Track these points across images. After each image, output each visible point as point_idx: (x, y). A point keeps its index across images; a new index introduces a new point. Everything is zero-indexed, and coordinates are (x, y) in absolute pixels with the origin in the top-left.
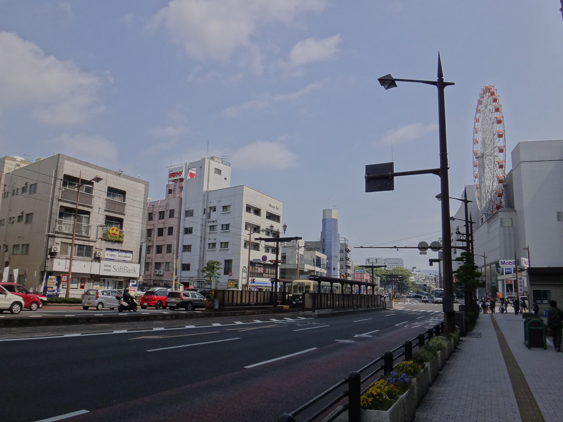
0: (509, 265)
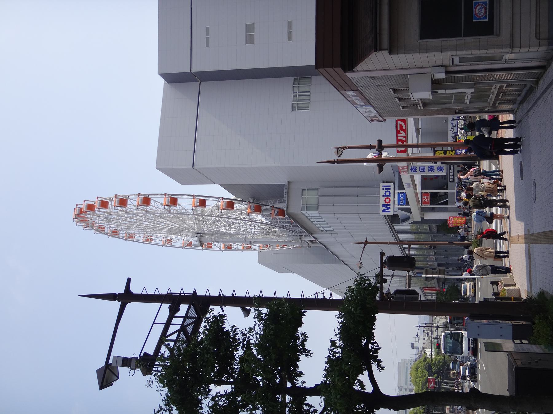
0: (391, 198)
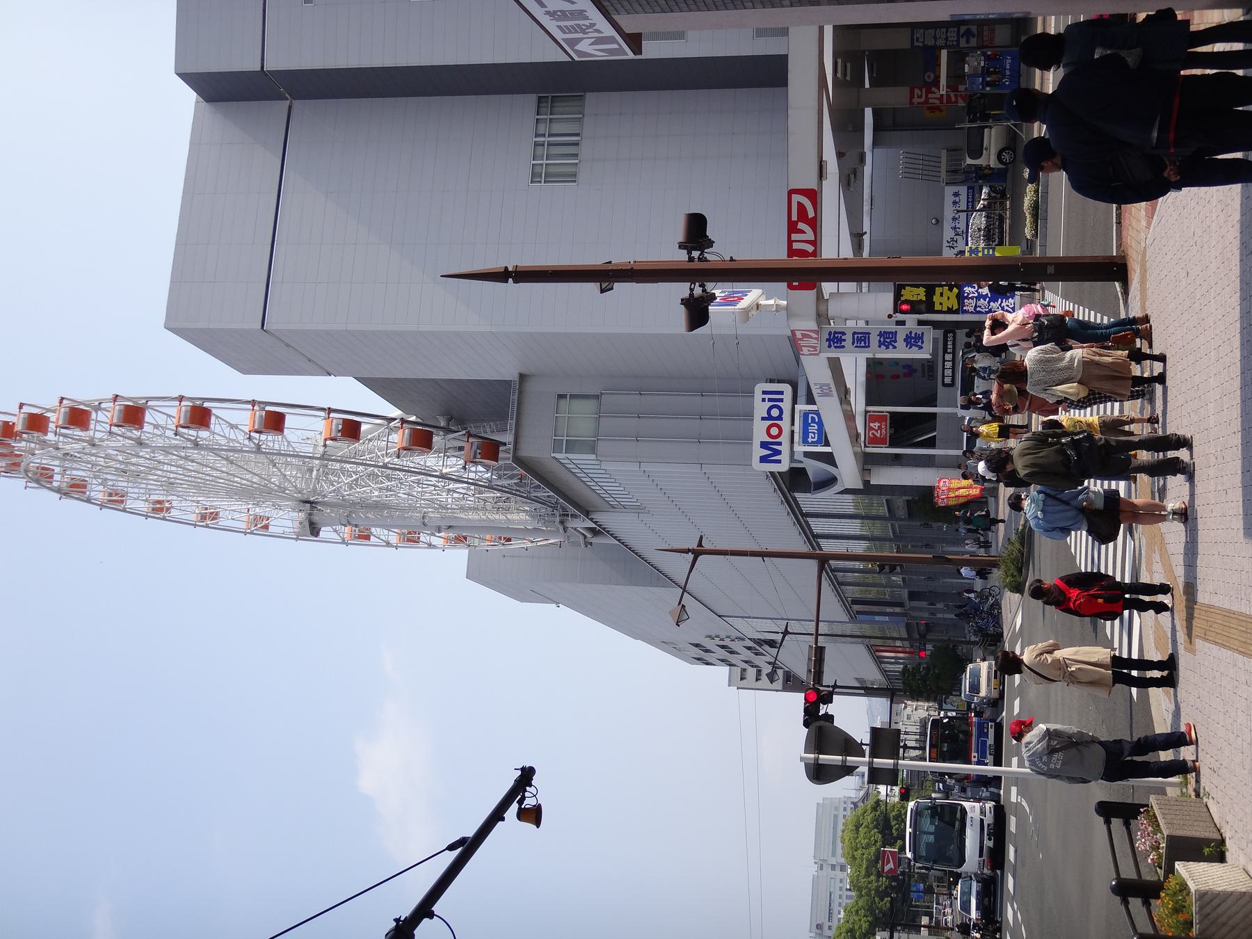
0: (785, 424)
